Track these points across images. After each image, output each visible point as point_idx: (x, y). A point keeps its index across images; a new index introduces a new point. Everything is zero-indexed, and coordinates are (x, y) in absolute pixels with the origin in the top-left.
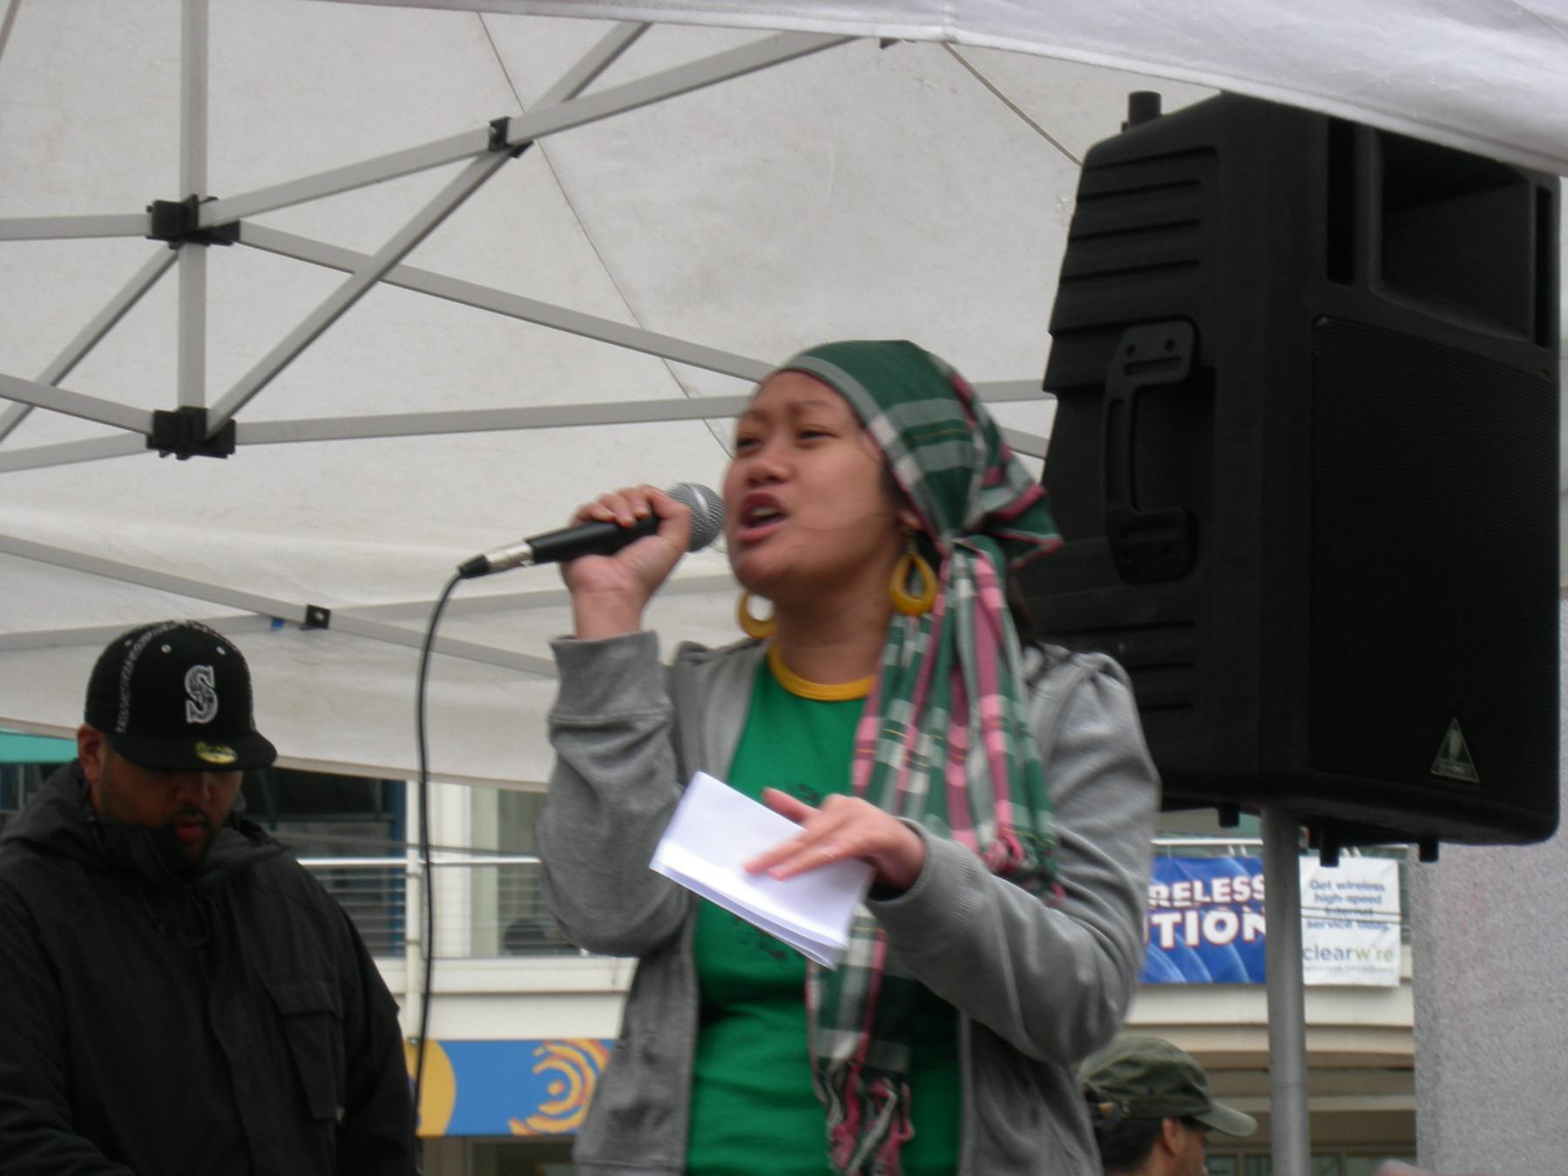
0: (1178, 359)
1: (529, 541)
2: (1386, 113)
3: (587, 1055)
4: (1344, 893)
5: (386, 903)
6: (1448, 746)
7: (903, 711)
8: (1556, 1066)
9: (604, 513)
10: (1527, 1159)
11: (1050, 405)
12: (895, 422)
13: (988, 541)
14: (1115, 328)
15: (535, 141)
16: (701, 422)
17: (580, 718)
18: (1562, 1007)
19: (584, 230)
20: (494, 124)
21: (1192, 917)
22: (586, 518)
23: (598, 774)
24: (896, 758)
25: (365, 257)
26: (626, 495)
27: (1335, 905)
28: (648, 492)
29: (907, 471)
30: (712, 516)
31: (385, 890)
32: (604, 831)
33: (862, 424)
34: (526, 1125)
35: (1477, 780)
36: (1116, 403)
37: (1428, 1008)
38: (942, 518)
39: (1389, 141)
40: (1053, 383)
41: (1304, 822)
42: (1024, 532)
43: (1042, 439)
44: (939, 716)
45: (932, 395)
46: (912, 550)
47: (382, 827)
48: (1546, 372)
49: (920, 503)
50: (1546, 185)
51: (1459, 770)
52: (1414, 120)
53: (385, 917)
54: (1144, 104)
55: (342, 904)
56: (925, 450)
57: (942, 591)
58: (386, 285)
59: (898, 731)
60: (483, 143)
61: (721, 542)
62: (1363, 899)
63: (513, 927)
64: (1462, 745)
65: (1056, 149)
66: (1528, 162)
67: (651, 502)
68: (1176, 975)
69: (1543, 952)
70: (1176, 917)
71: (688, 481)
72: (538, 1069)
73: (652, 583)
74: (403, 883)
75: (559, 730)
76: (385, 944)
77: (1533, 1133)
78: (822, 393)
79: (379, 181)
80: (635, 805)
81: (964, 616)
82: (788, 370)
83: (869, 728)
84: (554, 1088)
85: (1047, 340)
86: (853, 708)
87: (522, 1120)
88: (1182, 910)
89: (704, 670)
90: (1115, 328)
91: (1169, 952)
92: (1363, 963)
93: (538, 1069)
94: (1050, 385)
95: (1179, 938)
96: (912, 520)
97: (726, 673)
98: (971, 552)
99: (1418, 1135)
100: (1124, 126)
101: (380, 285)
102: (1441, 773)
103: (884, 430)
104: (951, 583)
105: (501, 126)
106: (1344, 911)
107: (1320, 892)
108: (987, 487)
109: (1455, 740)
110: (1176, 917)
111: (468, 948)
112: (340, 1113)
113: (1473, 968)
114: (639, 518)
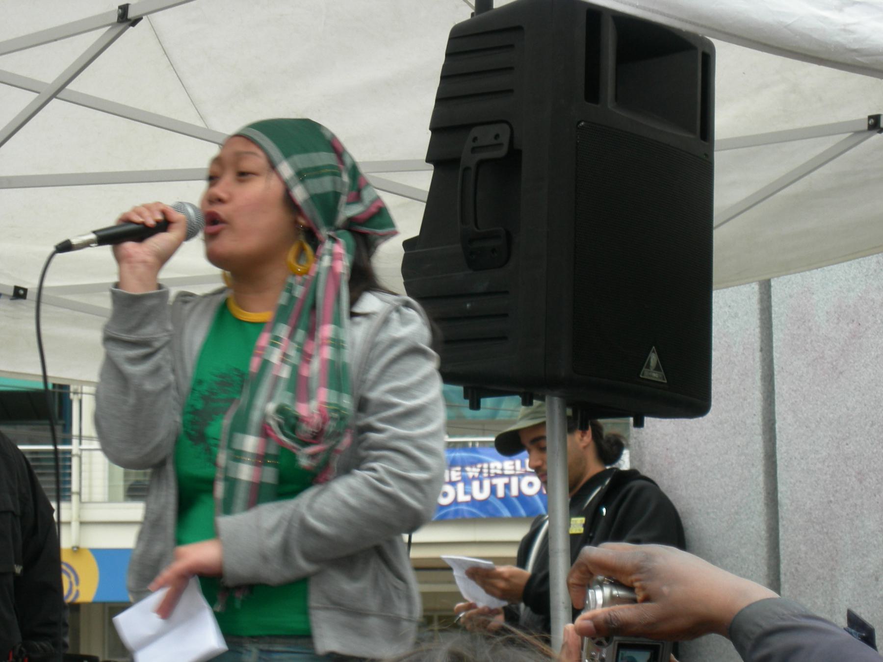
0: (501, 145)
1: (94, 232)
7: (283, 330)
9: (138, 219)
12: (293, 165)
13: (347, 235)
14: (467, 127)
15: (144, 17)
17: (122, 335)
19: (174, 69)
20: (120, 7)
21: (514, 480)
22: (126, 220)
23: (131, 369)
24: (275, 357)
25: (46, 84)
26: (148, 207)
28: (162, 207)
29: (299, 194)
30: (197, 222)
32: (132, 400)
33: (273, 166)
36: (467, 169)
38: (320, 220)
43: (425, 192)
44: (301, 334)
45: (317, 150)
46: (302, 238)
48: (706, 155)
49: (306, 210)
52: (637, 7)
56: (309, 182)
57: (315, 262)
58: (59, 100)
59: (277, 341)
60: (115, 19)
61: (201, 235)
67: (164, 213)
68: (506, 513)
70: (506, 480)
71: (184, 200)
73: (164, 258)
75: (109, 339)
78: (254, 149)
79: (56, 40)
80: (148, 386)
81: (322, 278)
82: (238, 135)
83: (264, 339)
85: (429, 134)
86: (260, 326)
88: (509, 476)
89: (188, 307)
90: (467, 127)
91: (501, 499)
94: (428, 160)
95: (507, 492)
96: (302, 221)
97: (200, 308)
98: (334, 240)
101: (54, 100)
103: (286, 170)
104: (318, 258)
105: (124, 9)
108: (349, 203)
110: (506, 480)
112: (18, 569)
114: (158, 222)
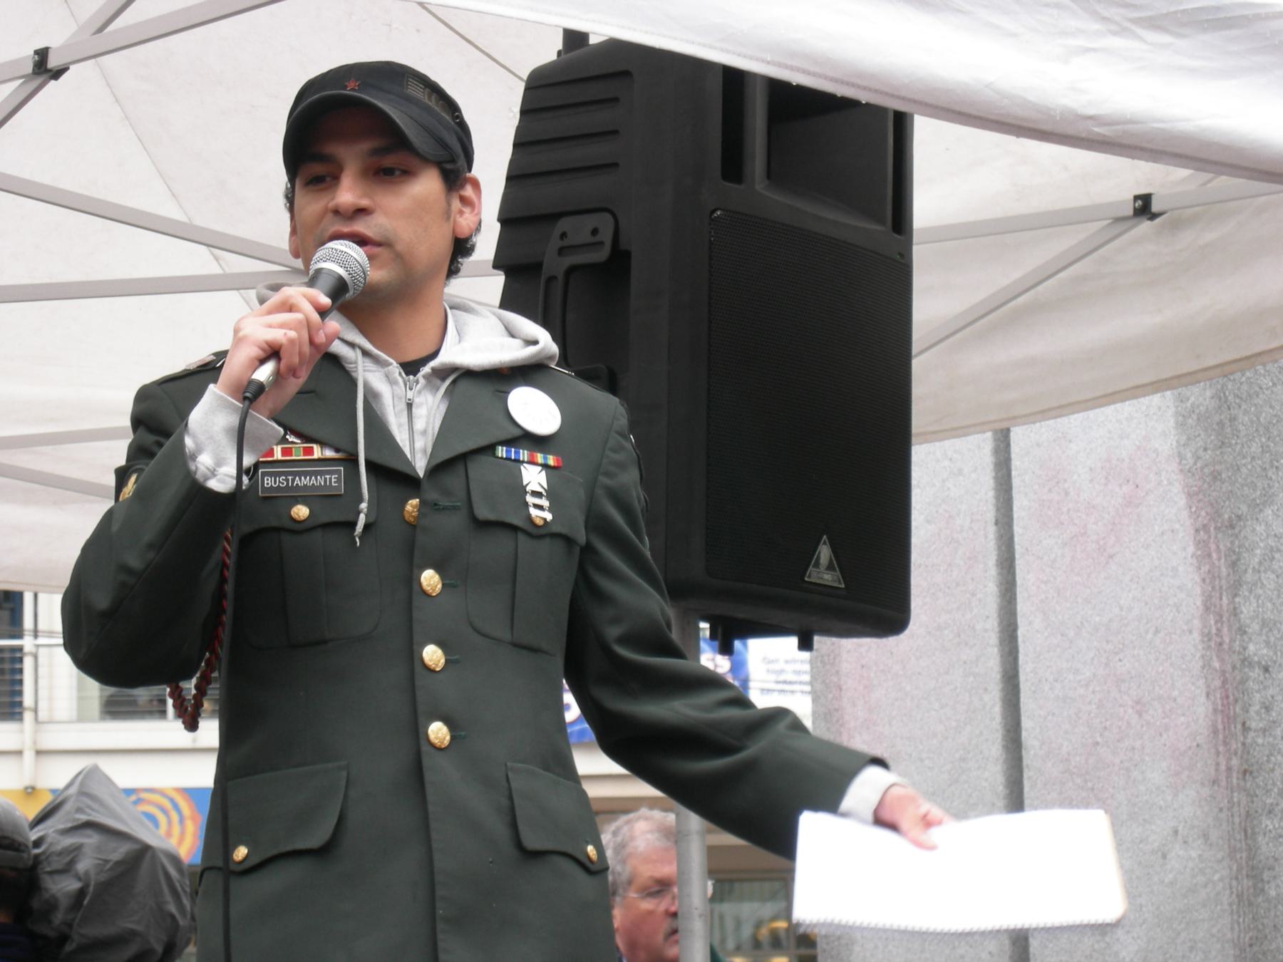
0: (601, 243)
3: (172, 800)
4: (790, 667)
5: (7, 677)
6: (818, 558)
15: (71, 67)
16: (236, 292)
20: (36, 52)
27: (782, 678)
31: (7, 666)
35: (843, 586)
36: (551, 279)
42: (444, 390)
53: (7, 688)
60: (29, 68)
64: (831, 560)
74: (21, 660)
76: (8, 710)
94: (497, 265)
100: (559, 53)
105: (42, 54)
106: (791, 683)
107: (771, 666)
109: (825, 553)
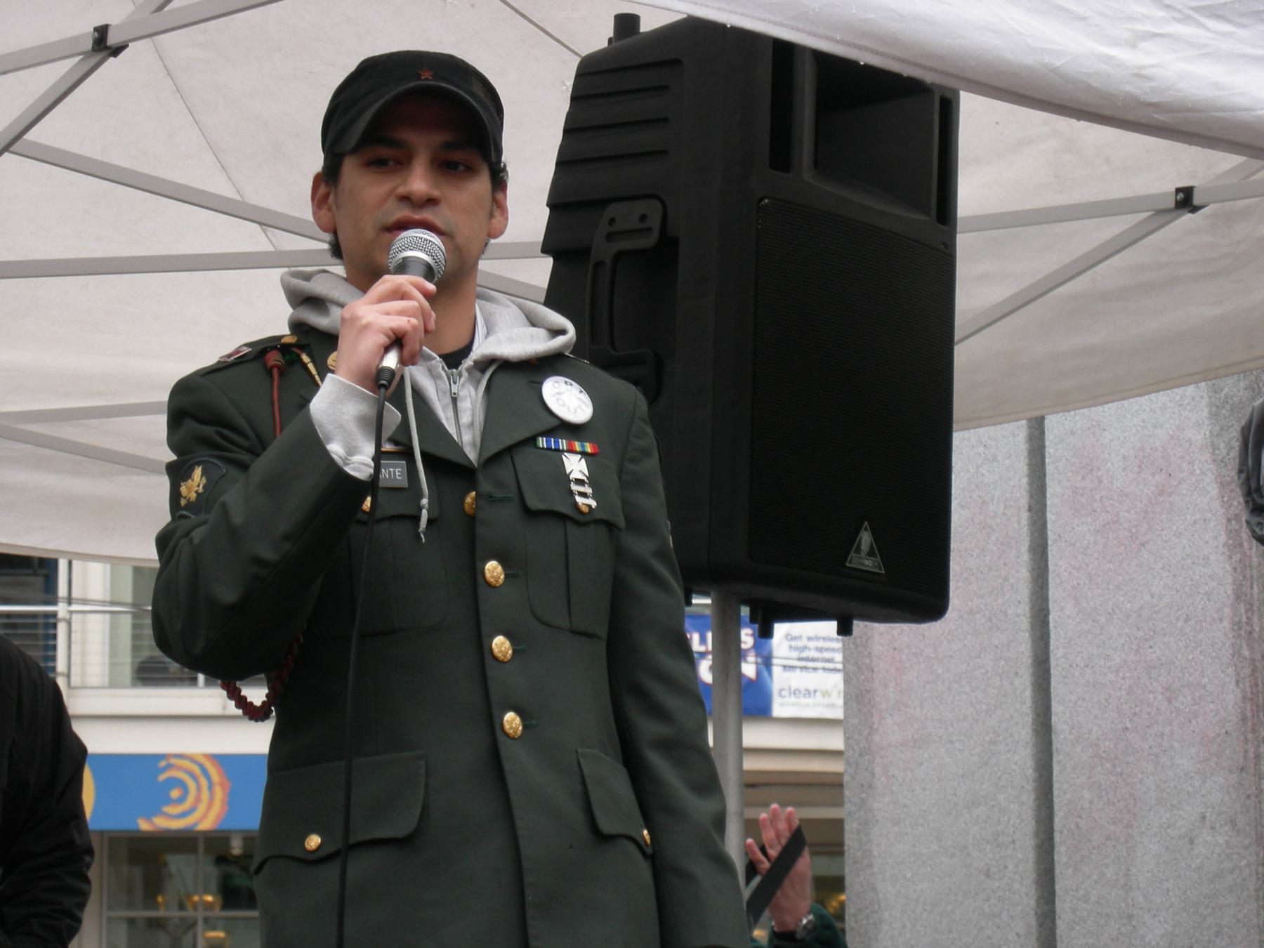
0: (650, 229)
2: (820, 37)
3: (201, 766)
4: (812, 644)
6: (860, 543)
8: (955, 795)
10: (932, 869)
11: (548, 262)
18: (961, 747)
20: (96, 29)
27: (804, 655)
31: (41, 631)
34: (152, 823)
36: (599, 264)
37: (855, 747)
39: (820, 57)
40: (548, 247)
41: (746, 603)
47: (39, 581)
50: (948, 95)
51: (869, 564)
54: (626, 24)
55: (16, 642)
60: (89, 45)
62: (828, 650)
63: (143, 663)
65: (567, 51)
66: (929, 78)
69: (947, 704)
72: (162, 777)
74: (55, 626)
77: (937, 849)
84: (175, 794)
85: (547, 211)
87: (149, 818)
92: (826, 700)
93: (162, 777)
94: (547, 249)
99: (846, 848)
100: (610, 40)
102: (853, 566)
105: (102, 32)
107: (793, 643)
109: (866, 538)
111: (106, 680)
113: (891, 715)
